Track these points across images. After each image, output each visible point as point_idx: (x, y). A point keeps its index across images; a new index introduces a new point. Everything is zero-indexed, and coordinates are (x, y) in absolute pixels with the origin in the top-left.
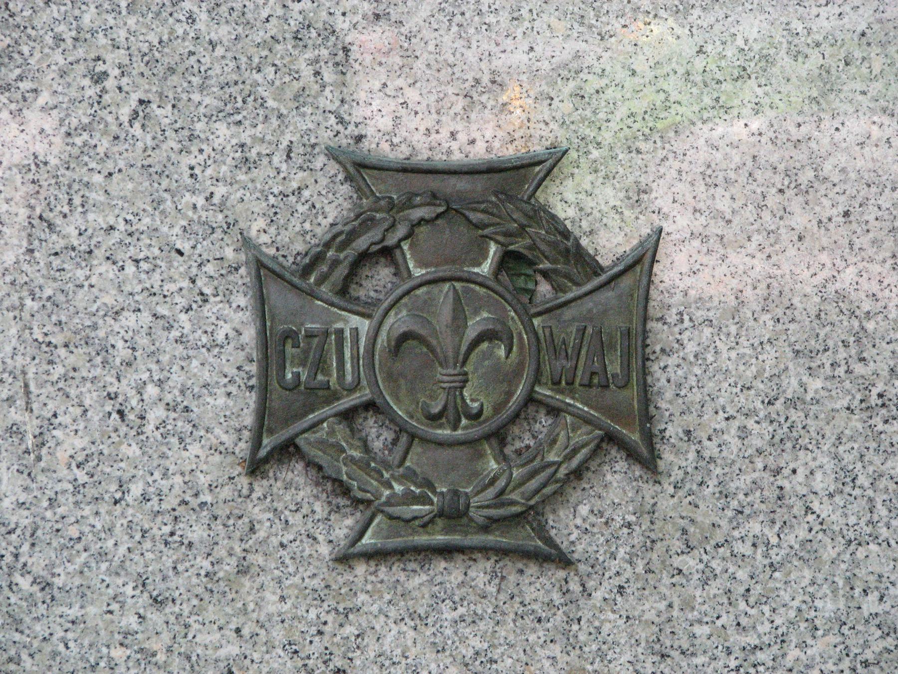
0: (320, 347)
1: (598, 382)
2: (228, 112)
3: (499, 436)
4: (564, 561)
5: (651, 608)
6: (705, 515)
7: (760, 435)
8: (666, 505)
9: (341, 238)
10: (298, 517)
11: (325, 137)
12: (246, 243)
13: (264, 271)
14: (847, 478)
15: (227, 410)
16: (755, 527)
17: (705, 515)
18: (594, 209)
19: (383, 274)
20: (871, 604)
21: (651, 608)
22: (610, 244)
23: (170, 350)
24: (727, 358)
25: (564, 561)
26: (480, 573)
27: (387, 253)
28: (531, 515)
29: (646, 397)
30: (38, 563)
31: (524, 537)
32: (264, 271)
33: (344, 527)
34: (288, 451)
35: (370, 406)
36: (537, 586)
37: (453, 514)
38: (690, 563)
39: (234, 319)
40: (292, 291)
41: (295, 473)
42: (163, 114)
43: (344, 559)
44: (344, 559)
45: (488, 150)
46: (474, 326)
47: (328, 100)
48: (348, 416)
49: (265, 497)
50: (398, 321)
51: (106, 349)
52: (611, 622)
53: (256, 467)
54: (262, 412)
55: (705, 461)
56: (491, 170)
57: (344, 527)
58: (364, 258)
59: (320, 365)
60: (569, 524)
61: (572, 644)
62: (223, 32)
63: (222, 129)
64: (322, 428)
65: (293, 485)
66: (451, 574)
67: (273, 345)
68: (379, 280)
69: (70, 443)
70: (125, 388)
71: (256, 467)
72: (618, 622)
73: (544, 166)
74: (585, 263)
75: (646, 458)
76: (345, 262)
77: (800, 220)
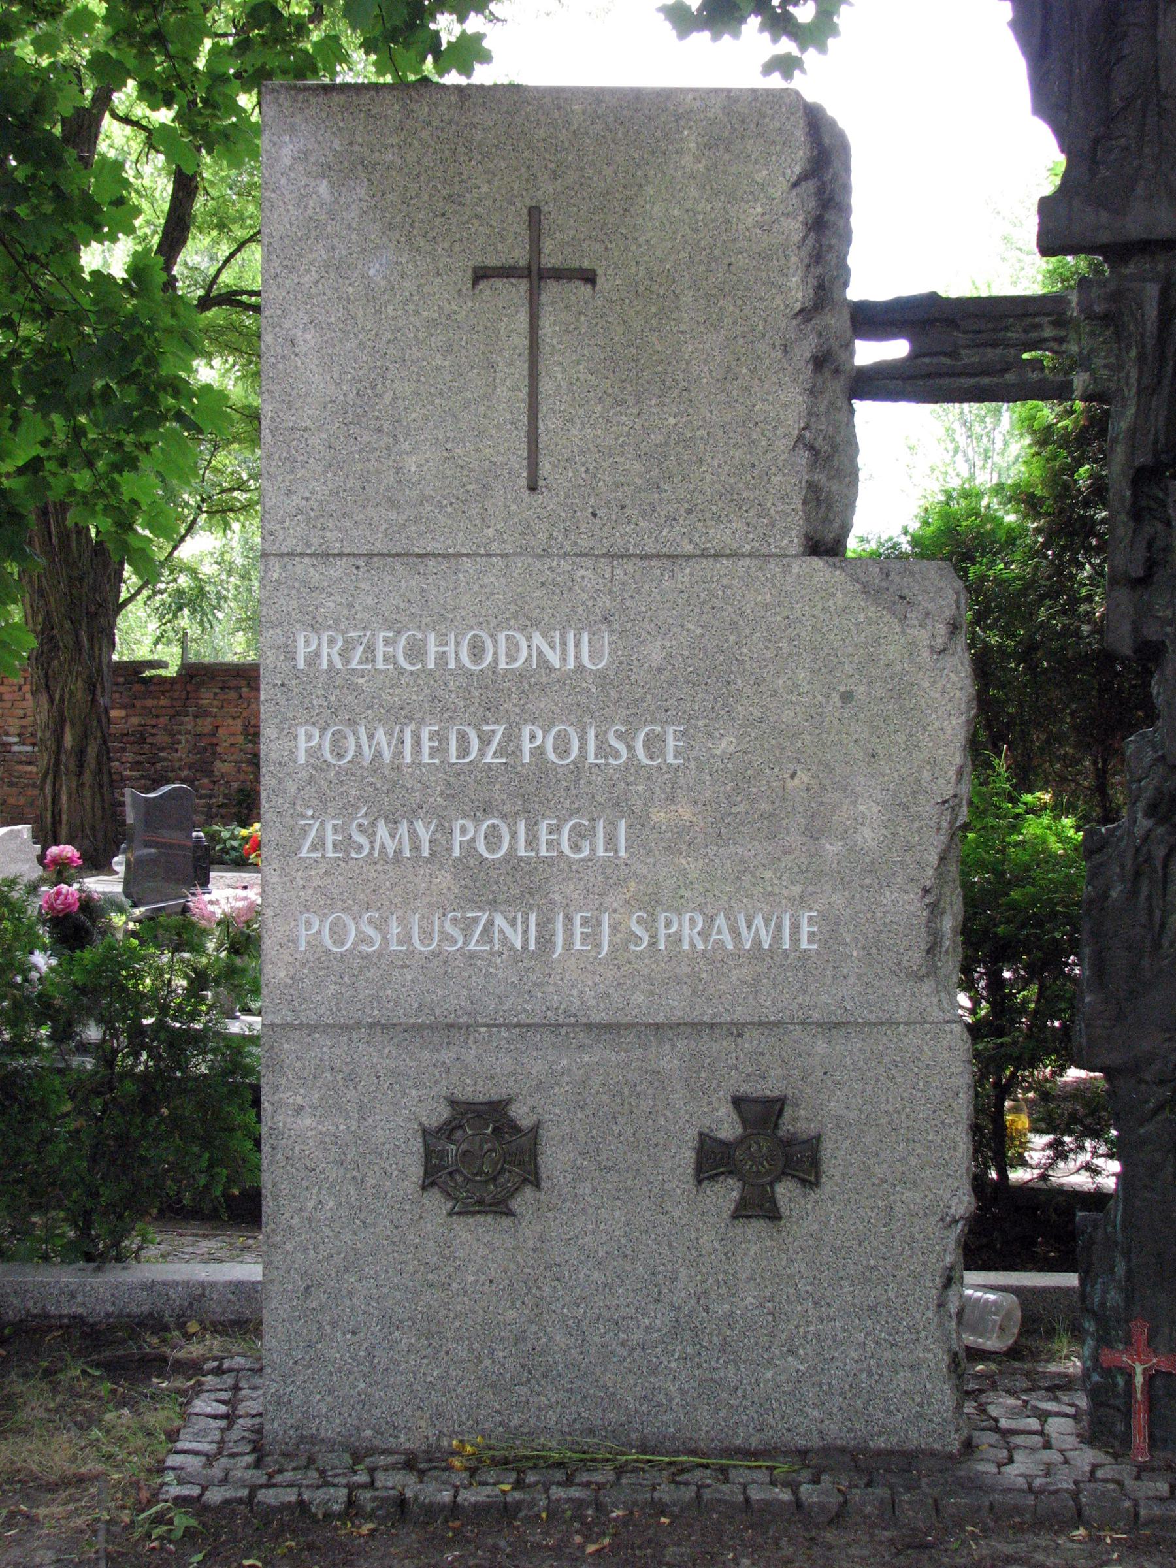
0: (441, 1155)
1: (521, 1164)
2: (415, 1086)
3: (494, 1179)
4: (513, 1215)
5: (539, 1228)
6: (554, 1201)
7: (570, 1177)
8: (543, 1198)
9: (447, 1123)
10: (436, 1204)
11: (443, 1093)
12: (421, 1124)
13: (426, 1132)
14: (595, 1189)
15: (416, 1171)
16: (568, 1204)
17: (554, 1201)
18: (521, 1114)
19: (460, 1132)
20: (602, 1226)
21: (539, 1228)
22: (526, 1123)
23: (399, 1155)
24: (560, 1155)
25: (513, 1215)
26: (489, 1218)
27: (461, 1127)
28: (504, 1201)
29: (536, 1166)
30: (362, 1217)
31: (502, 1208)
32: (426, 1132)
33: (450, 1205)
34: (433, 1184)
35: (457, 1171)
36: (506, 1222)
37: (481, 1202)
38: (549, 1214)
39: (417, 1145)
40: (434, 1140)
41: (436, 1189)
42: (397, 1087)
43: (450, 1214)
44: (450, 1214)
45: (998, 412)
46: (486, 1147)
47: (444, 1083)
48: (451, 1174)
49: (600, 1388)
50: (464, 1146)
51: (381, 1154)
52: (528, 1232)
53: (424, 1188)
54: (426, 1173)
55: (554, 1186)
56: (490, 1103)
57: (450, 1205)
58: (454, 1129)
59: (442, 1159)
60: (515, 1204)
61: (516, 1238)
62: (414, 1064)
63: (414, 1092)
64: (443, 1176)
65: (435, 1194)
66: (481, 1219)
67: (428, 1153)
68: (459, 1134)
69: (370, 1182)
70: (386, 1165)
71: (424, 1188)
72: (529, 1233)
73: (509, 1101)
74: (516, 1129)
75: (537, 1185)
76: (448, 1130)
77: (580, 1115)
